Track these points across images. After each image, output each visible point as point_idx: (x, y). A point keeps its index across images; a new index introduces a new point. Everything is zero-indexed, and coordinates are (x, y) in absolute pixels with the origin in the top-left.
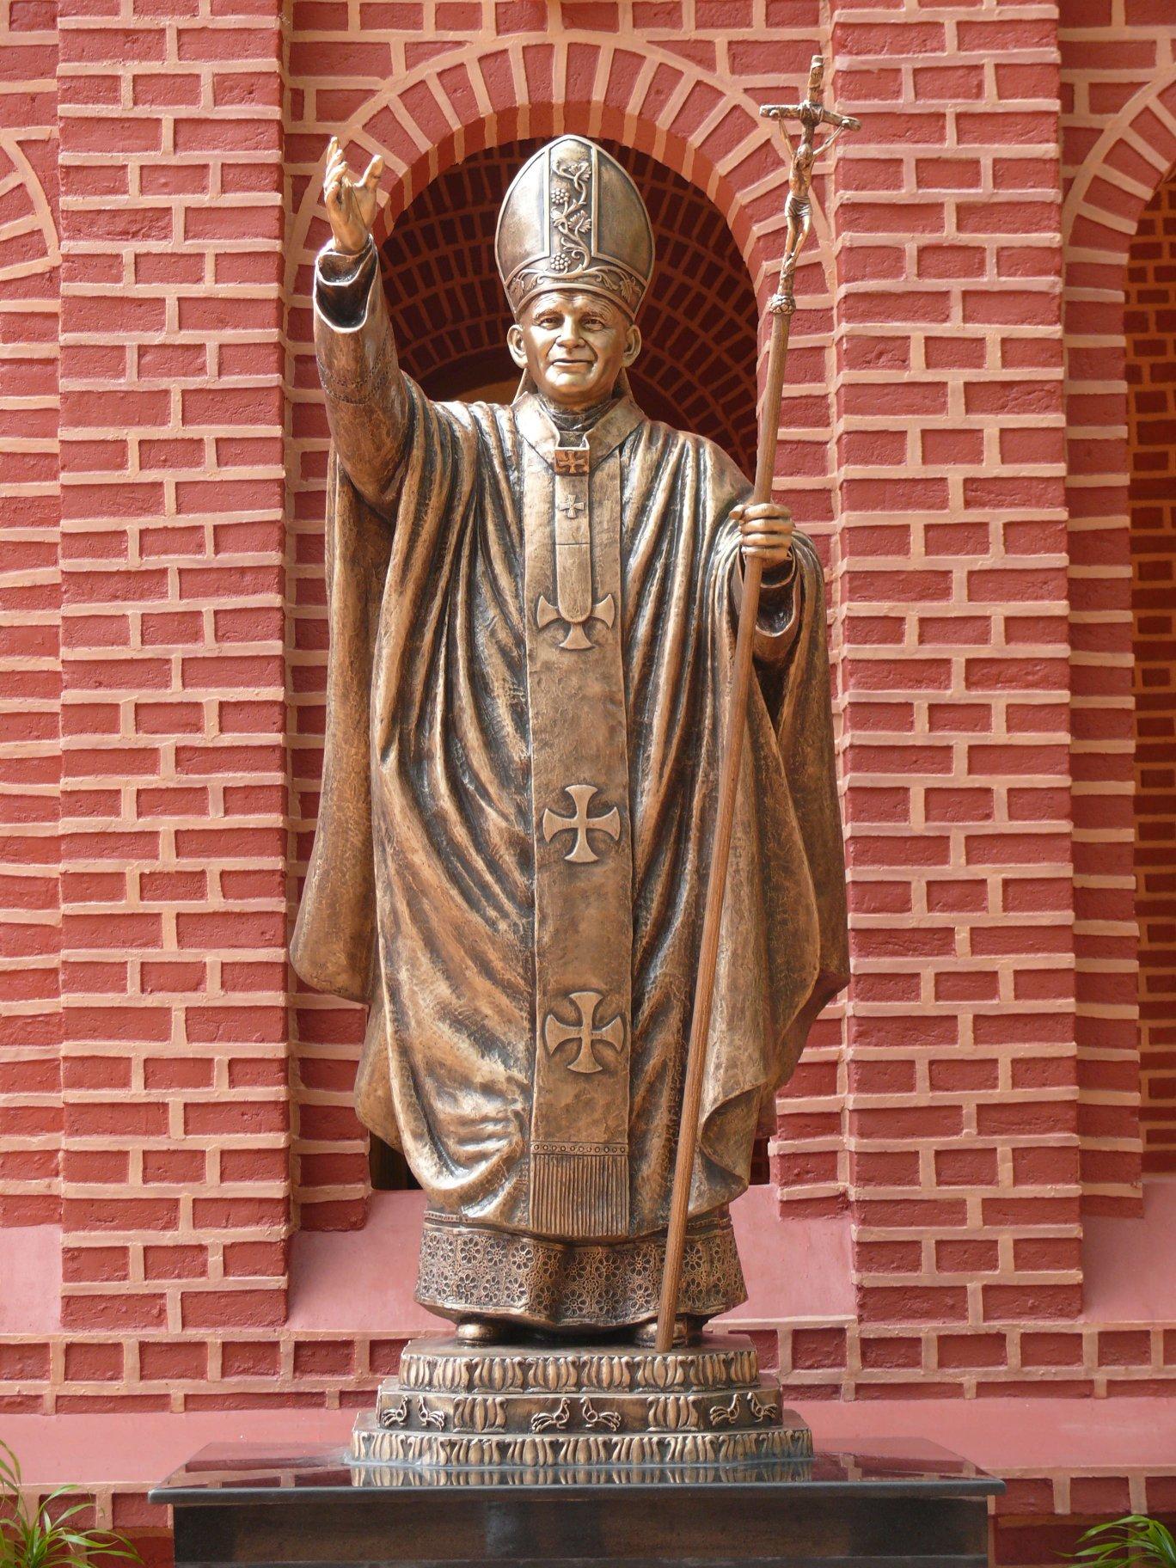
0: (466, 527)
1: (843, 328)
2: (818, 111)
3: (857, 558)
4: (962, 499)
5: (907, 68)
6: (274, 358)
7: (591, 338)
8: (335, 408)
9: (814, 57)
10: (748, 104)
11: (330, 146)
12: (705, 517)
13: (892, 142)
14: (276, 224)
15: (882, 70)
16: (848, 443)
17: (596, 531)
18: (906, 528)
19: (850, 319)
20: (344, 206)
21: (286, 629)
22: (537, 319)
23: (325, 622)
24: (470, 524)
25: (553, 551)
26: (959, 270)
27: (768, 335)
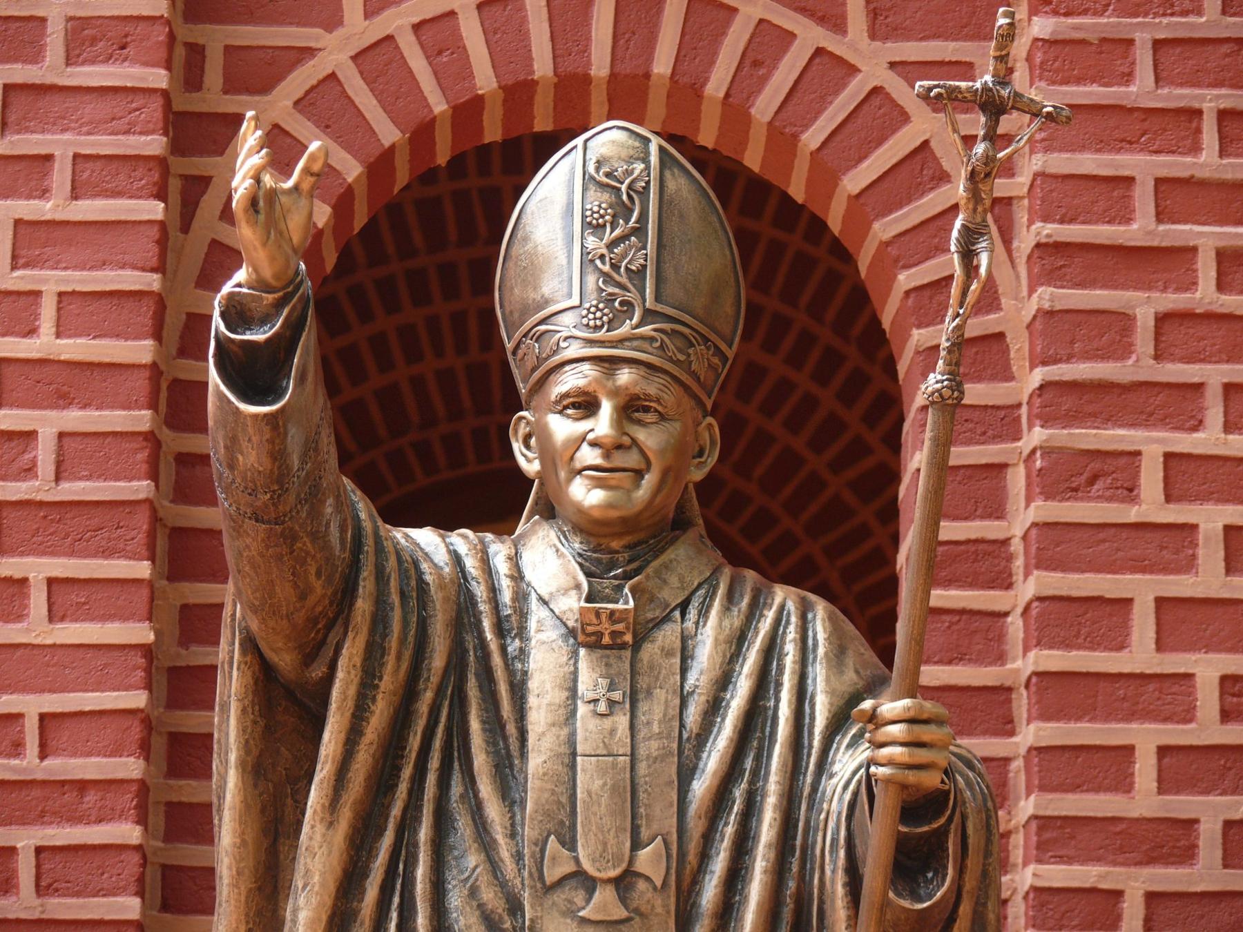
0: (436, 722)
1: (1036, 436)
2: (1005, 93)
3: (1050, 796)
4: (1217, 707)
5: (1143, 40)
6: (142, 456)
7: (641, 435)
8: (238, 530)
9: (1001, 10)
10: (895, 86)
11: (245, 124)
12: (813, 718)
13: (1119, 151)
14: (155, 249)
15: (1104, 40)
16: (1040, 615)
17: (640, 736)
18: (1130, 749)
19: (1046, 422)
20: (262, 217)
21: (148, 879)
22: (557, 402)
23: (210, 871)
24: (443, 719)
25: (573, 766)
26: (1220, 352)
27: (918, 445)
